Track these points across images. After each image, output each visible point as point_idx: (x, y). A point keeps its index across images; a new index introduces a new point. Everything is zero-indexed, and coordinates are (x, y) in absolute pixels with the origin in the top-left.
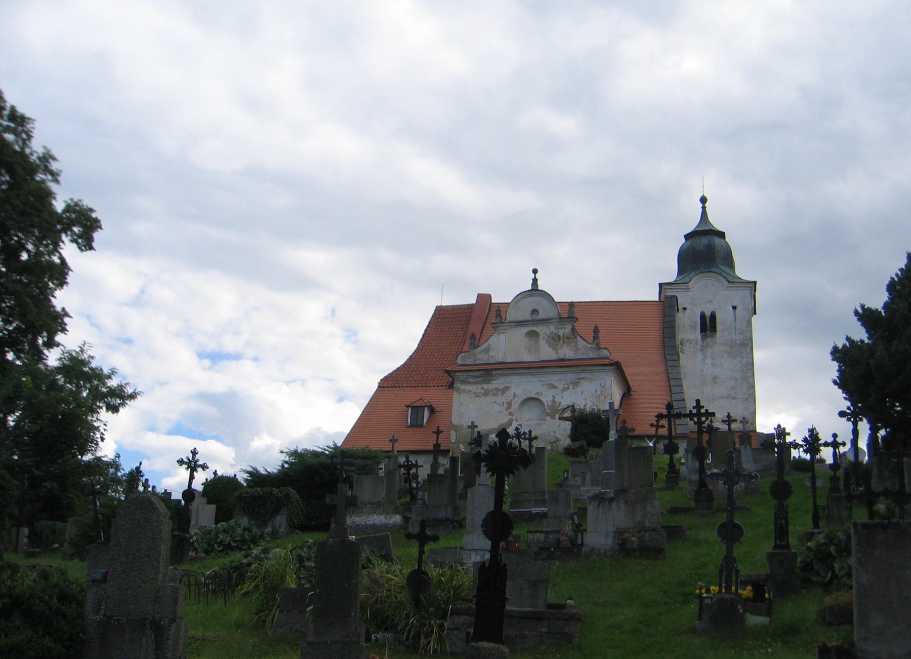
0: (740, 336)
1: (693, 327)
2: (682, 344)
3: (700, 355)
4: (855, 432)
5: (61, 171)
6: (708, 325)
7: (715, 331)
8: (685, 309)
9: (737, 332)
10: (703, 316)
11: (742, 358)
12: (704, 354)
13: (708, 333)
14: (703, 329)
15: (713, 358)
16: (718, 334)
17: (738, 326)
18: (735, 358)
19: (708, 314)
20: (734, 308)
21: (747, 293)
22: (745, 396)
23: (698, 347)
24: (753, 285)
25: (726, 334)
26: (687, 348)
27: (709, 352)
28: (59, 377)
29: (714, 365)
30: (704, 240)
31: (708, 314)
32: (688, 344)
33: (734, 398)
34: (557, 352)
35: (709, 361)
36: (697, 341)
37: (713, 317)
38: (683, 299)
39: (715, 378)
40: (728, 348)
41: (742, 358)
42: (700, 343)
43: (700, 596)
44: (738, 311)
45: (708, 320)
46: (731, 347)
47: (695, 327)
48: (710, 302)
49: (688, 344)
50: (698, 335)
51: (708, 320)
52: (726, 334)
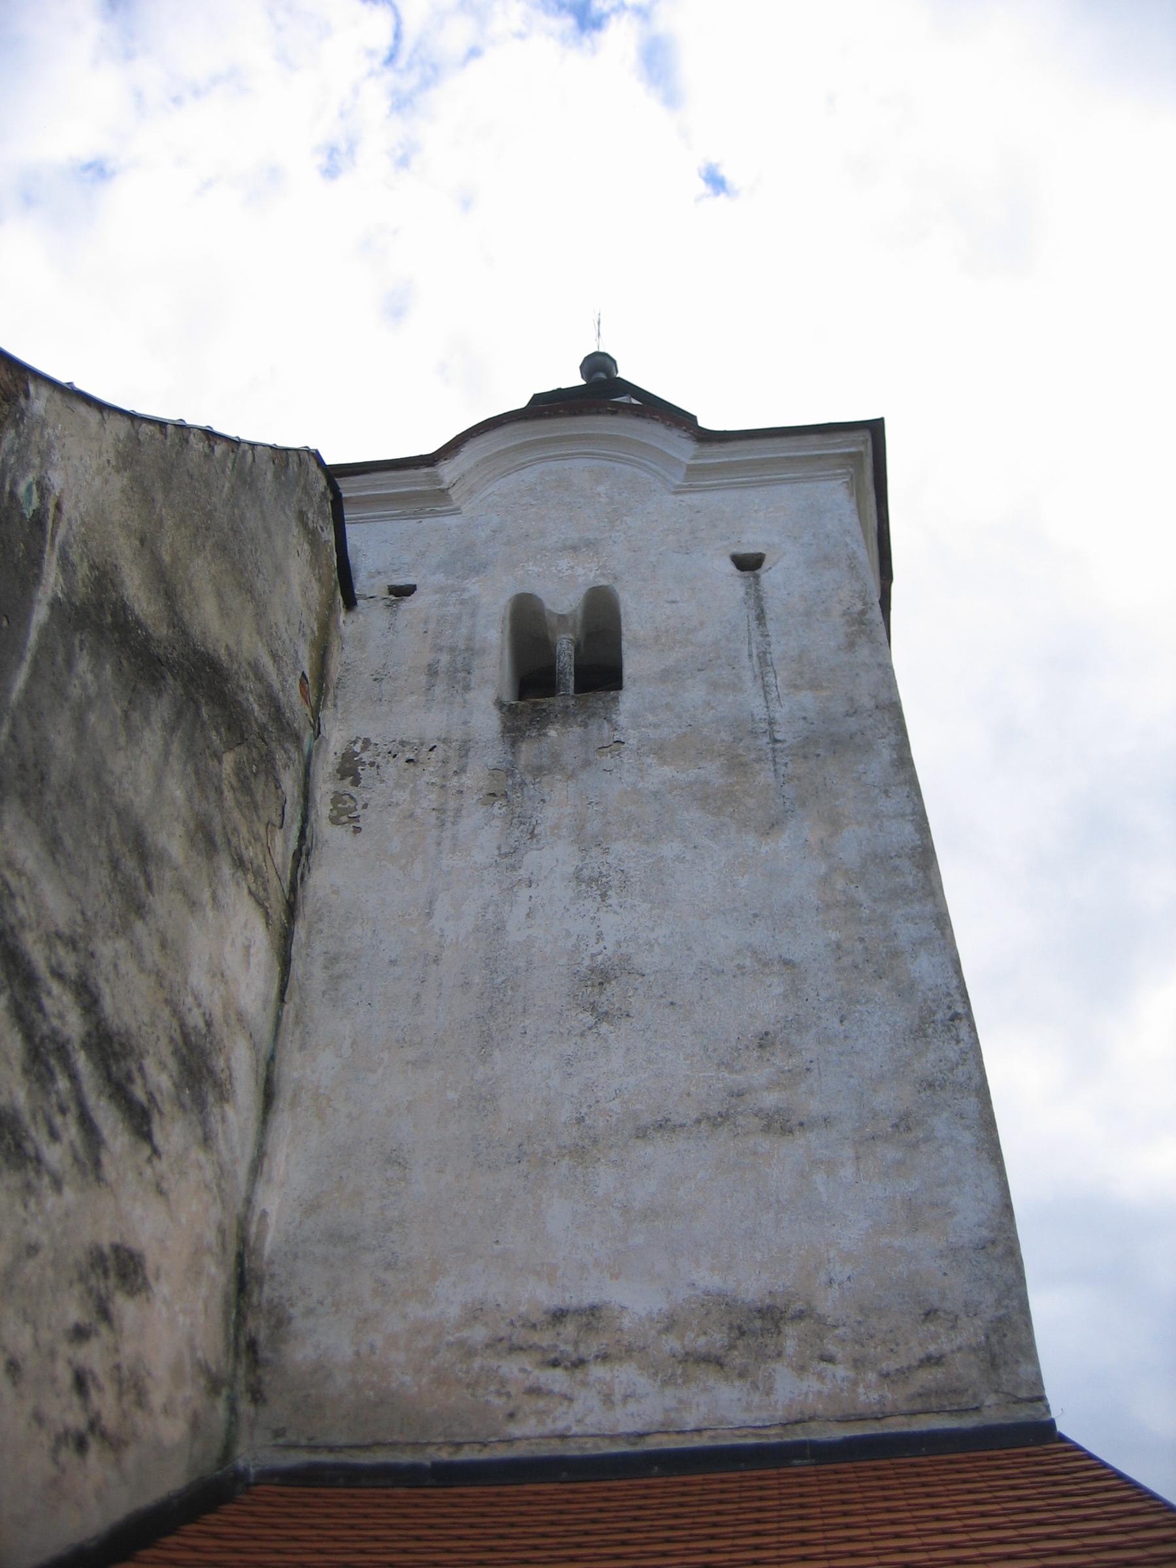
3: (481, 832)
5: (594, 52)
8: (402, 592)
11: (835, 822)
16: (628, 699)
18: (773, 826)
20: (748, 564)
21: (835, 497)
22: (890, 1099)
23: (475, 777)
24: (861, 444)
25: (695, 693)
27: (557, 803)
29: (594, 885)
33: (780, 1124)
34: (34, 467)
37: (602, 619)
39: (602, 977)
40: (712, 771)
41: (835, 822)
42: (490, 751)
44: (770, 576)
46: (737, 765)
49: (391, 770)
50: (482, 711)
52: (695, 693)
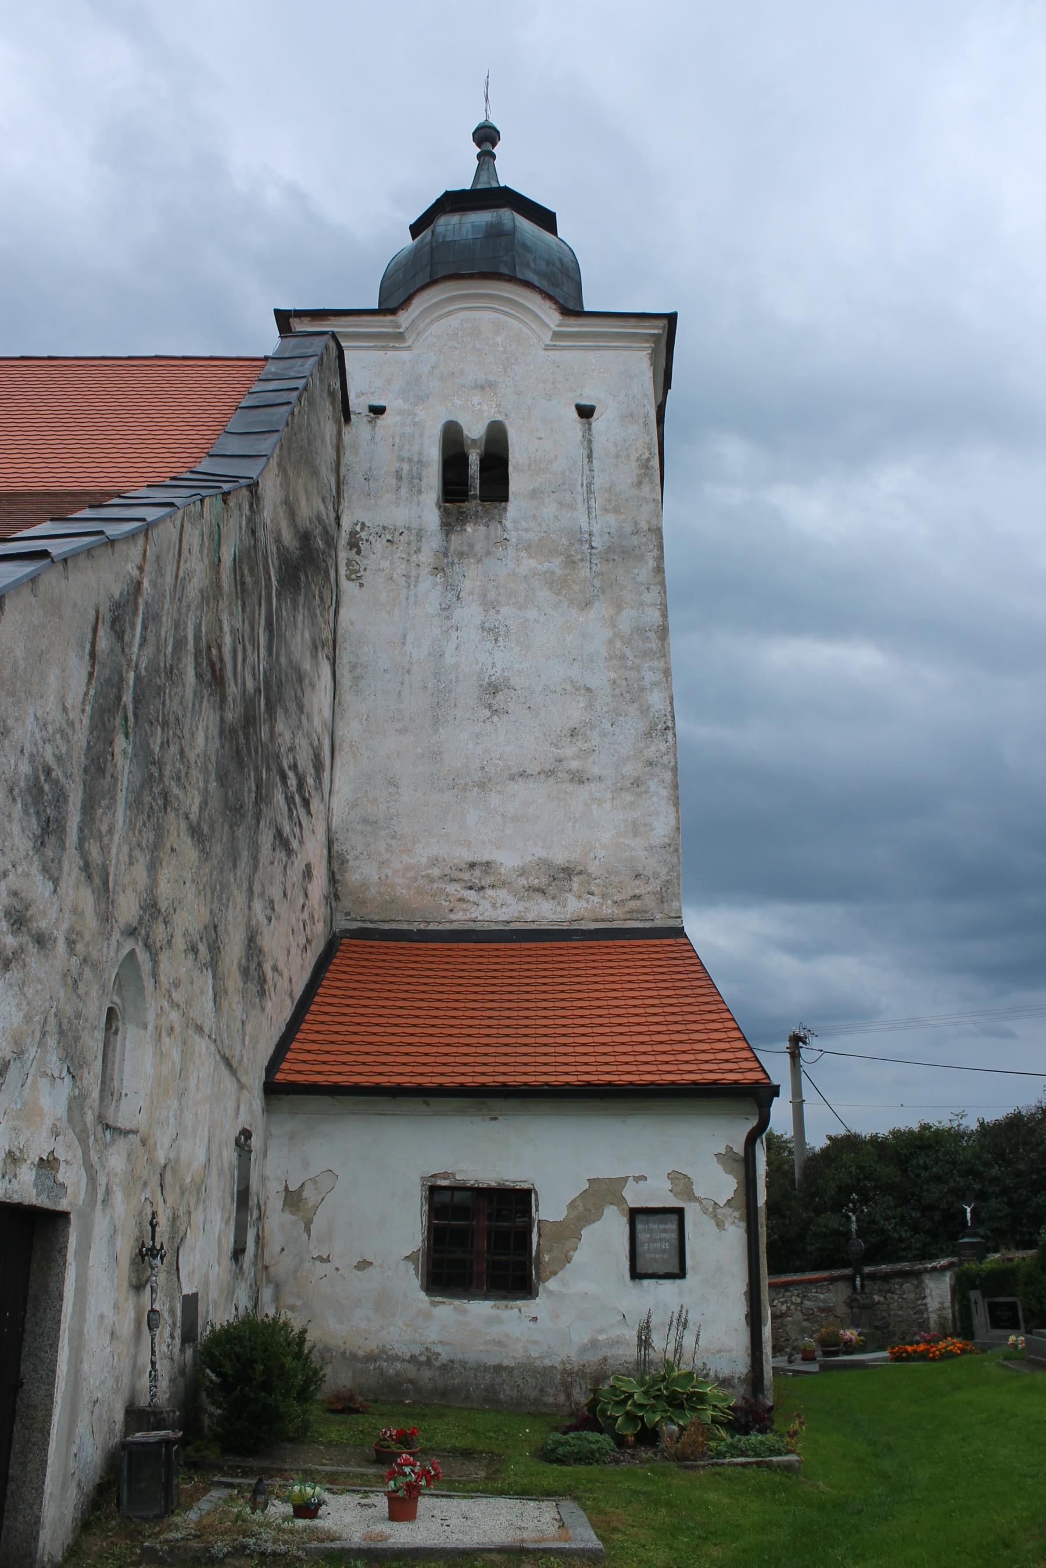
0: (611, 519)
1: (408, 480)
2: (354, 544)
3: (430, 590)
4: (220, 1484)
6: (475, 476)
7: (504, 498)
8: (378, 411)
9: (597, 504)
10: (452, 439)
12: (450, 586)
13: (473, 505)
14: (454, 487)
15: (489, 605)
16: (514, 507)
17: (600, 481)
18: (587, 605)
19: (474, 430)
20: (585, 412)
21: (640, 363)
23: (426, 557)
25: (549, 509)
26: (377, 557)
27: (471, 578)
28: (1012, 1338)
29: (492, 632)
30: (481, 218)
31: (474, 430)
32: (379, 545)
33: (579, 778)
35: (470, 613)
36: (420, 535)
38: (367, 372)
39: (494, 689)
40: (555, 565)
42: (434, 541)
43: (714, 1421)
44: (598, 423)
45: (474, 458)
46: (570, 562)
47: (415, 482)
48: (485, 387)
49: (379, 545)
50: (427, 508)
51: (474, 458)
52: (549, 509)
